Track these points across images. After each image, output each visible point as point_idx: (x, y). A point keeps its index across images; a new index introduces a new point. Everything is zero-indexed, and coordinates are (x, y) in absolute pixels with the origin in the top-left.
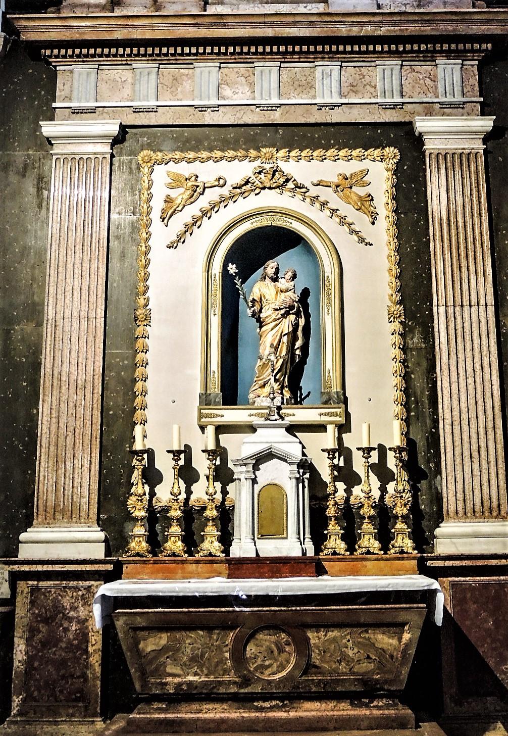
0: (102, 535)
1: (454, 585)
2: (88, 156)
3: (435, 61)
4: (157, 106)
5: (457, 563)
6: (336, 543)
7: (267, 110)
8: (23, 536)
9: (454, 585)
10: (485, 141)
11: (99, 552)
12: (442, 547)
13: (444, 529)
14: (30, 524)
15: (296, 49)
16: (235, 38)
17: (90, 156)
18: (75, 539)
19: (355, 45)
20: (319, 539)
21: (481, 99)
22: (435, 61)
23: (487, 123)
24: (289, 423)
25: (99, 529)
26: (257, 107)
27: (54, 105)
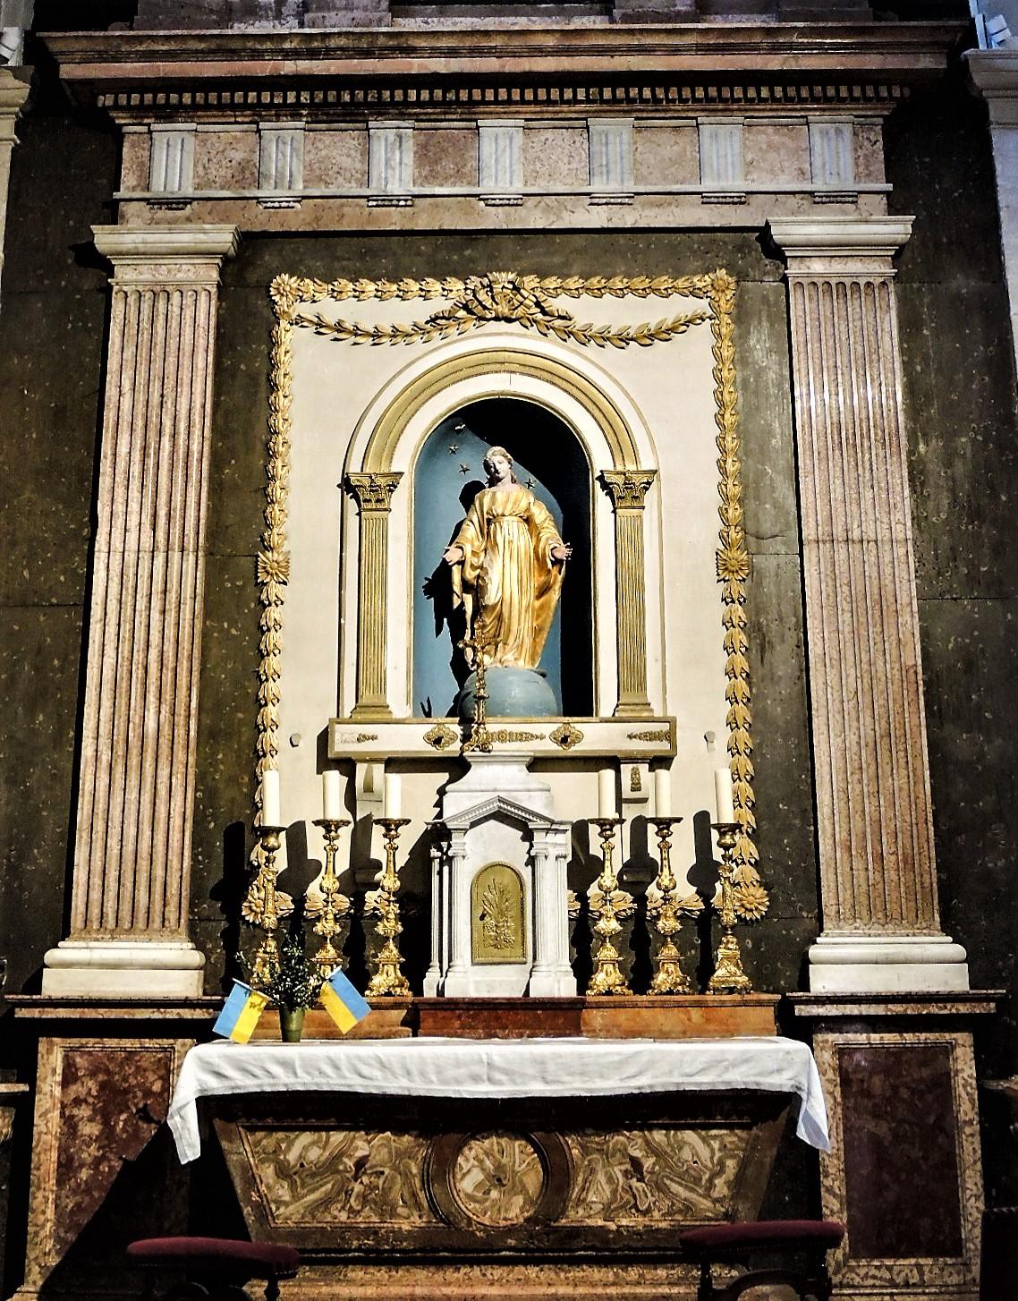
0: (197, 958)
1: (842, 1052)
2: (838, 280)
3: (476, 120)
4: (747, 193)
5: (897, 1009)
6: (609, 976)
7: (280, 207)
8: (51, 956)
9: (842, 1052)
10: (896, 259)
11: (187, 985)
12: (823, 980)
13: (64, 952)
14: (65, 933)
15: (631, 95)
16: (115, 80)
17: (842, 280)
18: (157, 962)
19: (791, 86)
20: (583, 968)
21: (890, 187)
22: (476, 120)
23: (899, 229)
24: (532, 754)
25: (950, 939)
26: (480, 200)
27: (117, 195)
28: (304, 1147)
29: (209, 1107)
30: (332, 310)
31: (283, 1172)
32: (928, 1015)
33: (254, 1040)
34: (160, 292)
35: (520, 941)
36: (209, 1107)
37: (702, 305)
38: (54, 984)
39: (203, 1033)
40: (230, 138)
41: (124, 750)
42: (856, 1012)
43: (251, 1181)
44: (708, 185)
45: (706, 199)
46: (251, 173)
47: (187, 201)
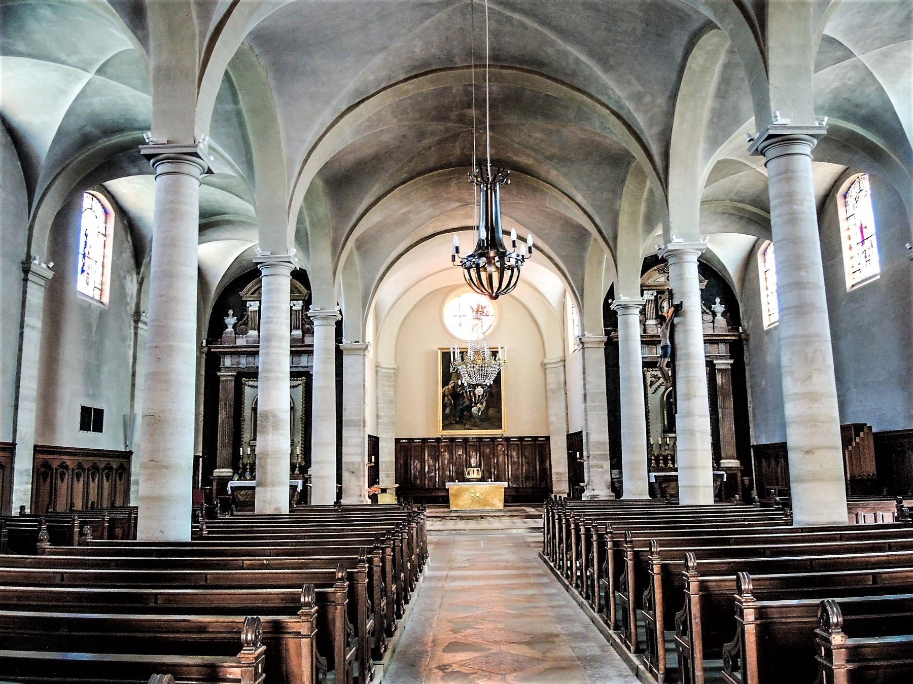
28: (243, 492)
29: (231, 487)
30: (251, 383)
31: (240, 495)
32: (86, 632)
33: (238, 480)
34: (226, 381)
35: (555, 578)
36: (231, 487)
37: (300, 382)
38: (214, 474)
39: (232, 480)
40: (236, 359)
41: (223, 443)
42: (236, 590)
43: (237, 496)
44: (302, 365)
45: (302, 367)
46: (238, 363)
47: (230, 367)
